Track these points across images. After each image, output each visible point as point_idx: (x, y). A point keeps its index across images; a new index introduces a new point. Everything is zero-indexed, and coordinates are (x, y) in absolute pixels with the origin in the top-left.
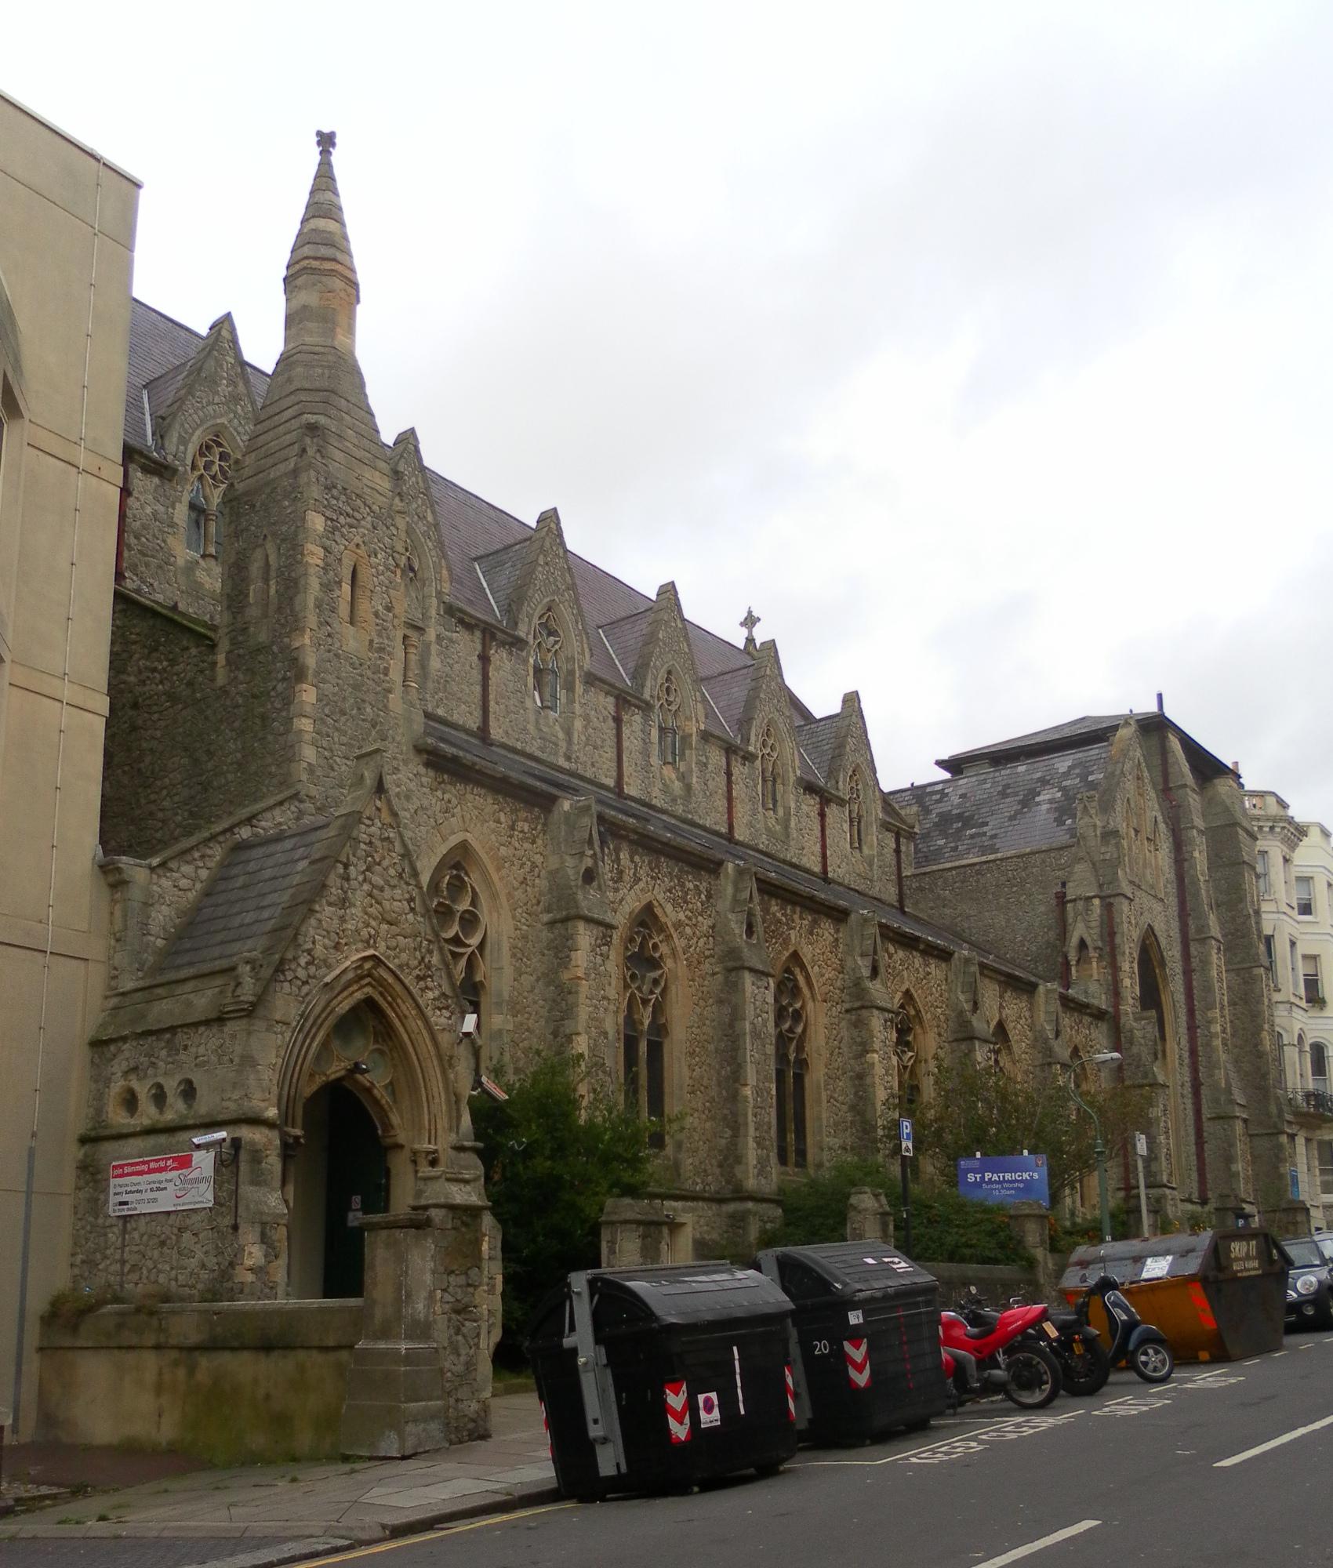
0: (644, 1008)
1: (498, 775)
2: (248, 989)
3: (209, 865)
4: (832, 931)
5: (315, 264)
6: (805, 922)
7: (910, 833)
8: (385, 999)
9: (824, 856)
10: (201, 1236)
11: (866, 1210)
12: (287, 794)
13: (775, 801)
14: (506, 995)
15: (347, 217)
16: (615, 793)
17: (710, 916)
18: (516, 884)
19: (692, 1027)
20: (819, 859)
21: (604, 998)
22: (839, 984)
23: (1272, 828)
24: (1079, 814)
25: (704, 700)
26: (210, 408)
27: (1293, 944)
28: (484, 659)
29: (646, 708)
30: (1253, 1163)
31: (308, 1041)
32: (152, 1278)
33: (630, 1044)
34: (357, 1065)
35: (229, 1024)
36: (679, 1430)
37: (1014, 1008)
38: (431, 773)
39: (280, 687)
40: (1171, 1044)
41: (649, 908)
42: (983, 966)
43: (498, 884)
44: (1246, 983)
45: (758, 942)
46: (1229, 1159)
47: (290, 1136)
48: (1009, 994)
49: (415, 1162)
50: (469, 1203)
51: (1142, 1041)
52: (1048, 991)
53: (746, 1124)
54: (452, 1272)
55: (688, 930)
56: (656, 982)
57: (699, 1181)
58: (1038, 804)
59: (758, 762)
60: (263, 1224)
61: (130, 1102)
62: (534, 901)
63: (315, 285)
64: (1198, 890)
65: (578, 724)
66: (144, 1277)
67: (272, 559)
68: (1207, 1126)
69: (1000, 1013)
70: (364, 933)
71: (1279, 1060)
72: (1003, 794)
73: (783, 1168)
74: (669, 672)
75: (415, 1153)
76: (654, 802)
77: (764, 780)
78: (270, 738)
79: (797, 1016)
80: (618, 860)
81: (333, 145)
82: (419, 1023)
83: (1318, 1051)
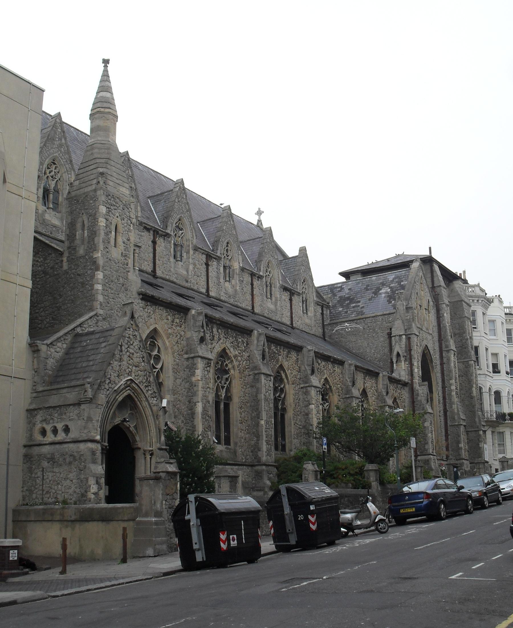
0: (223, 390)
1: (169, 302)
2: (90, 394)
3: (66, 342)
4: (296, 355)
5: (102, 110)
6: (285, 352)
7: (328, 306)
8: (135, 395)
9: (292, 317)
10: (74, 481)
11: (310, 470)
12: (92, 314)
13: (271, 294)
14: (171, 388)
15: (114, 91)
16: (205, 295)
17: (248, 352)
18: (174, 343)
19: (241, 397)
20: (290, 319)
21: (208, 387)
22: (298, 377)
23: (478, 301)
24: (397, 299)
25: (242, 252)
26: (52, 150)
27: (487, 349)
28: (154, 242)
29: (218, 259)
30: (468, 443)
31: (109, 411)
32: (55, 496)
33: (217, 404)
34: (125, 419)
35: (82, 405)
36: (224, 546)
37: (370, 383)
38: (143, 302)
39: (89, 272)
40: (435, 396)
41: (224, 350)
42: (356, 367)
43: (167, 343)
44: (466, 367)
45: (267, 362)
46: (459, 442)
47: (104, 446)
48: (368, 377)
49: (145, 454)
50: (173, 471)
51: (422, 395)
52: (384, 376)
53: (262, 436)
54: (168, 494)
55: (239, 358)
56: (227, 379)
57: (244, 458)
58: (381, 294)
59: (264, 279)
60: (97, 477)
61: (44, 432)
62: (181, 350)
63: (102, 117)
64: (446, 330)
65: (191, 267)
66: (51, 495)
67: (86, 222)
68: (449, 428)
69: (364, 386)
70: (127, 371)
71: (481, 399)
72: (367, 289)
73: (277, 452)
74: (228, 243)
75: (145, 451)
76: (222, 298)
77: (267, 286)
78: (85, 291)
79: (282, 390)
80: (212, 332)
81: (108, 63)
82: (146, 403)
83: (498, 394)
